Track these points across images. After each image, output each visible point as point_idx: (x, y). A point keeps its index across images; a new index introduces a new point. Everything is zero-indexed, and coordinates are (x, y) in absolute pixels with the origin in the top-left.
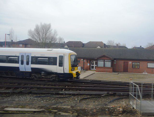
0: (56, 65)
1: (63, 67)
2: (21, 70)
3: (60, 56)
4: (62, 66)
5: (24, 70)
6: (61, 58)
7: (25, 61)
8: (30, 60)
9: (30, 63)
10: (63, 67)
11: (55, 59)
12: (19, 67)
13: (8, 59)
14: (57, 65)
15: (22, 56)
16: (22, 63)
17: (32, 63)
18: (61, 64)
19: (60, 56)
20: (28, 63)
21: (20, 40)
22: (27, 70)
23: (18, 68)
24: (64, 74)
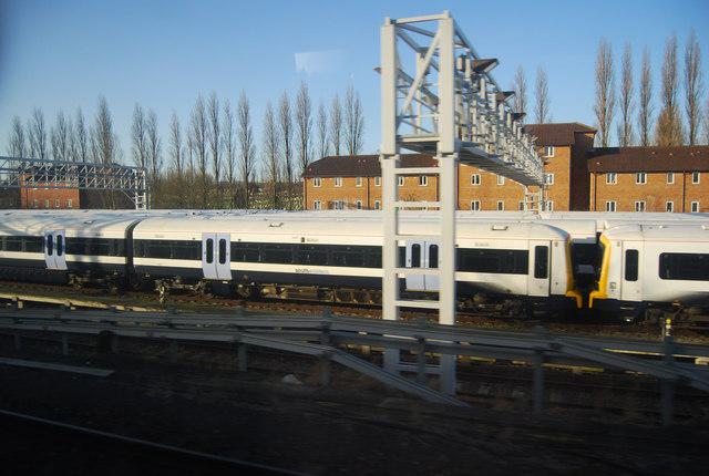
0: (525, 271)
1: (548, 280)
2: (51, 266)
3: (537, 248)
4: (545, 277)
5: (213, 277)
6: (542, 253)
7: (216, 253)
8: (64, 244)
9: (228, 257)
10: (548, 280)
11: (41, 238)
12: (407, 281)
13: (15, 242)
14: (527, 273)
15: (50, 237)
16: (210, 260)
17: (235, 258)
18: (542, 272)
19: (537, 248)
20: (222, 260)
21: (553, 122)
22: (60, 268)
23: (200, 271)
24: (553, 298)
